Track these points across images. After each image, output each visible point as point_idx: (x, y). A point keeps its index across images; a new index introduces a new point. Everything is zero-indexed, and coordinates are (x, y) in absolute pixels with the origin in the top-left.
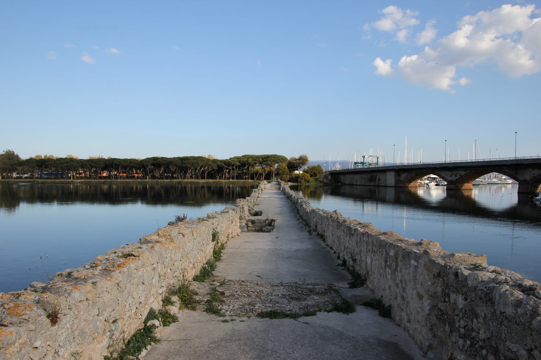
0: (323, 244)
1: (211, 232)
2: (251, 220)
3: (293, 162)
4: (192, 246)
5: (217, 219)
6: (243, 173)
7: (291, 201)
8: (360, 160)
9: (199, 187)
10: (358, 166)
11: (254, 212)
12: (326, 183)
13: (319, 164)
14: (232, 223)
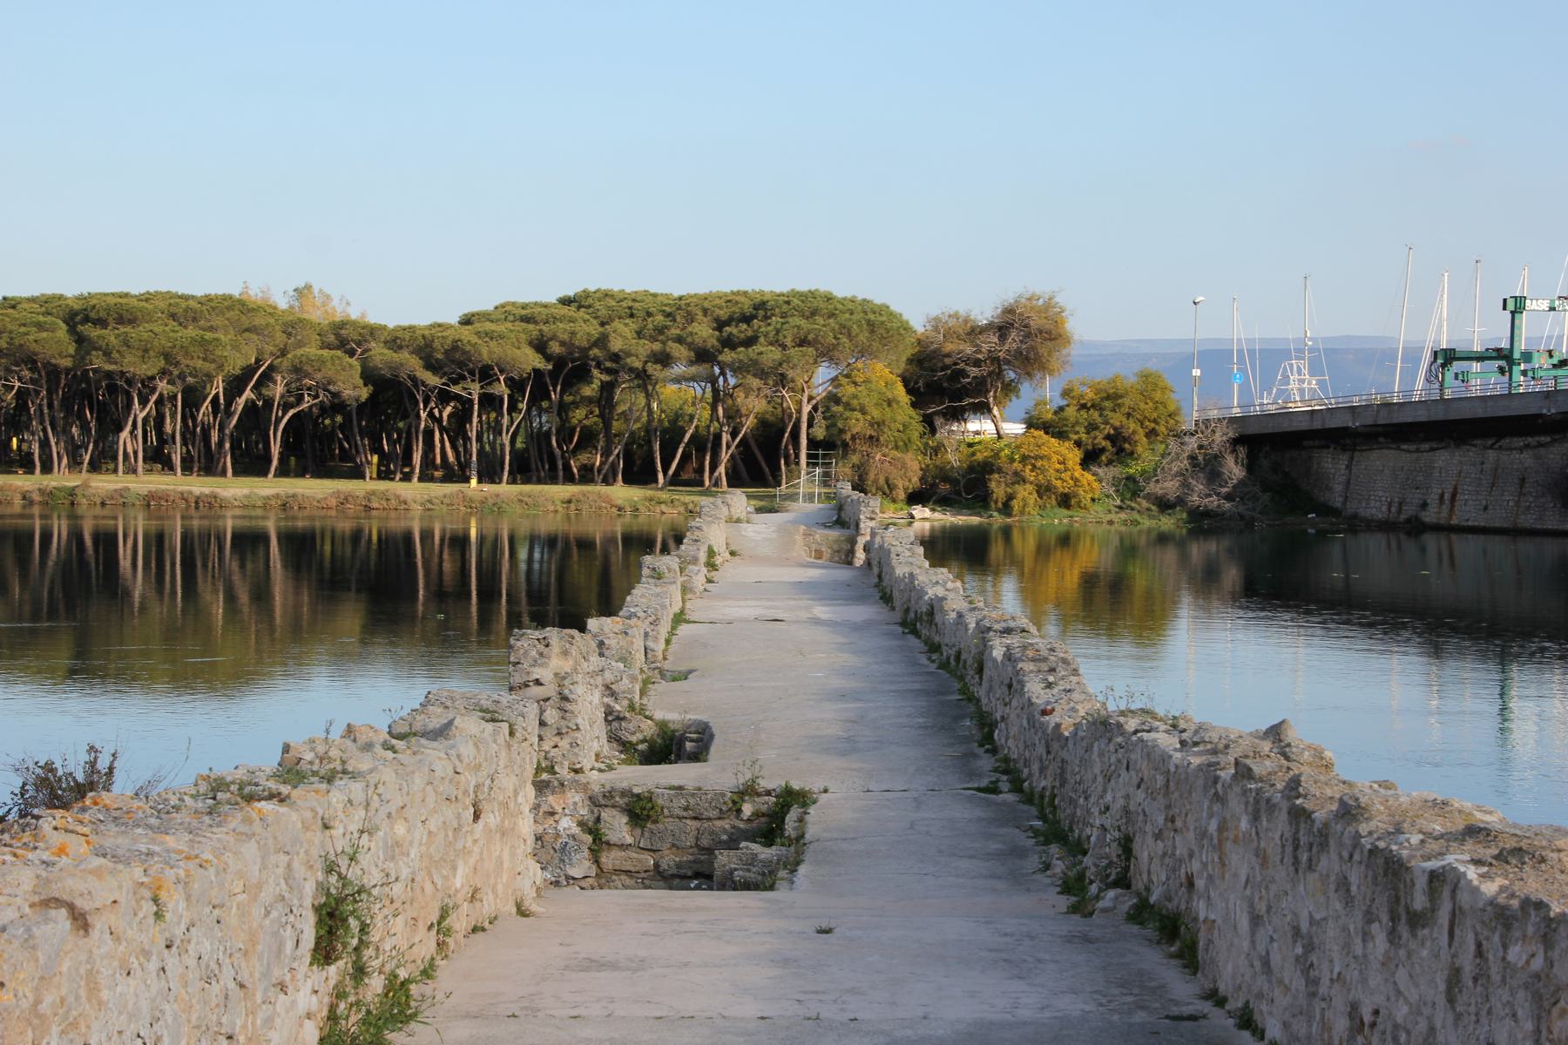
0: (1183, 990)
1: (309, 888)
2: (624, 793)
3: (949, 347)
4: (145, 1006)
5: (356, 789)
6: (565, 433)
7: (934, 648)
8: (1487, 331)
9: (220, 540)
10: (1462, 377)
11: (649, 729)
12: (1207, 514)
13: (1152, 366)
14: (477, 817)
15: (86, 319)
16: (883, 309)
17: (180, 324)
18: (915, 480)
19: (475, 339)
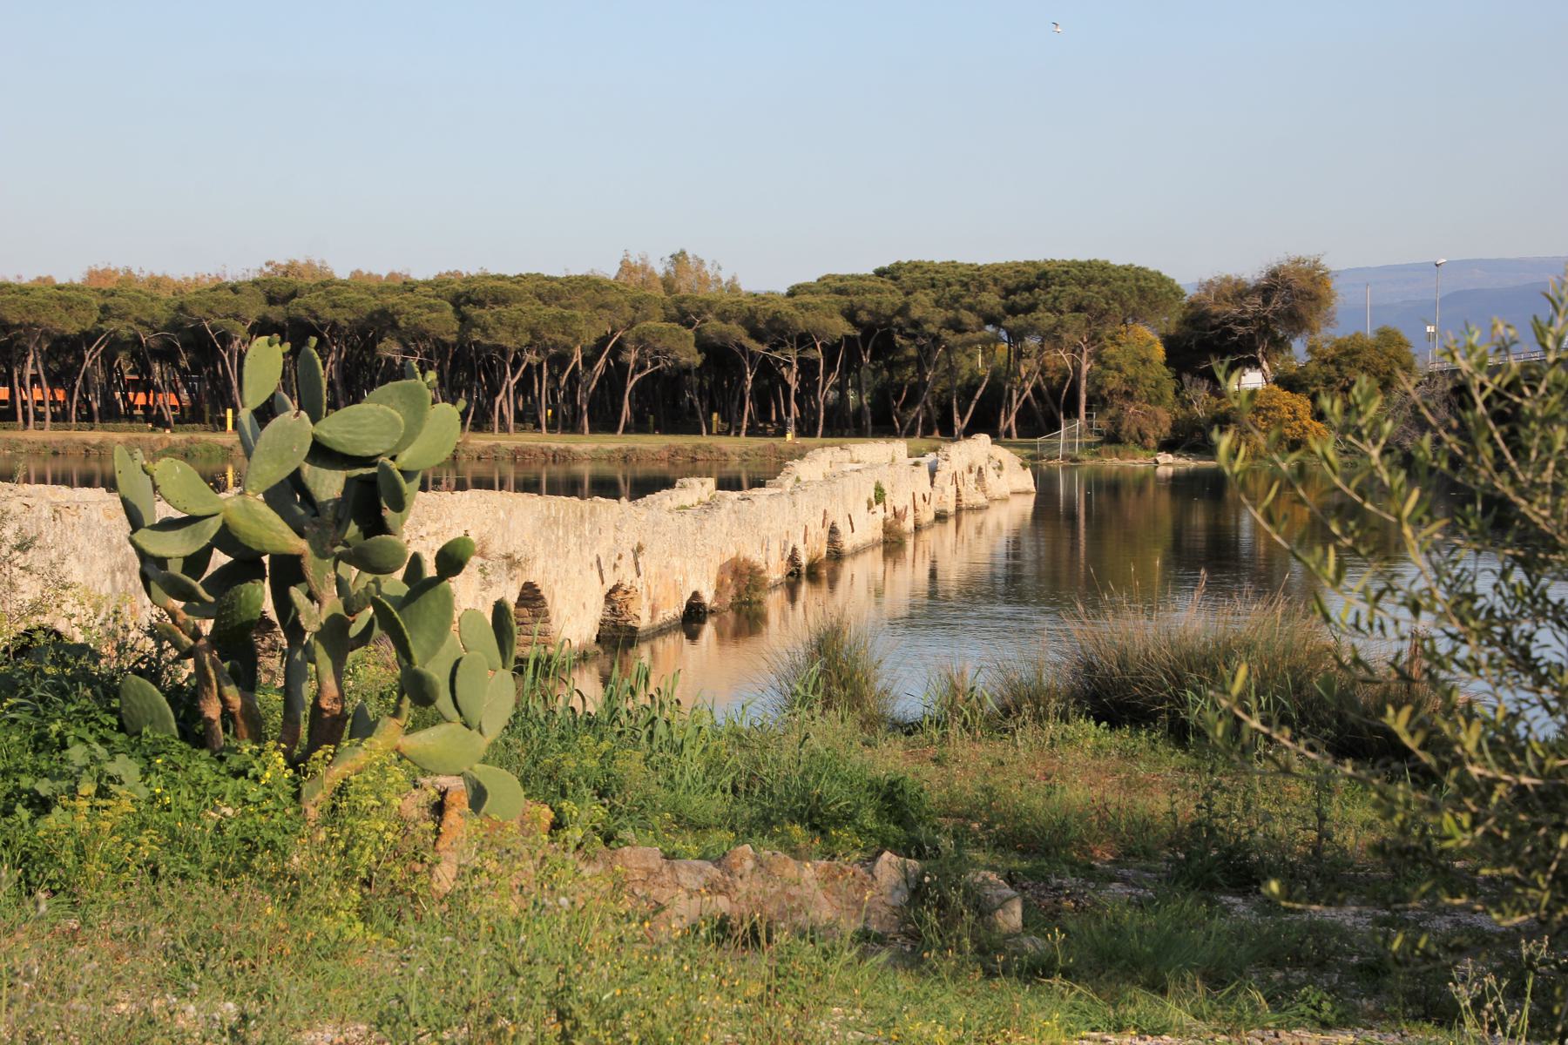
3: (1216, 309)
15: (469, 301)
16: (1161, 279)
17: (545, 303)
18: (1166, 429)
19: (792, 311)
